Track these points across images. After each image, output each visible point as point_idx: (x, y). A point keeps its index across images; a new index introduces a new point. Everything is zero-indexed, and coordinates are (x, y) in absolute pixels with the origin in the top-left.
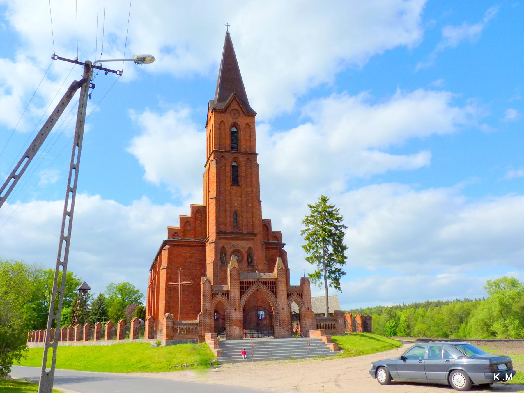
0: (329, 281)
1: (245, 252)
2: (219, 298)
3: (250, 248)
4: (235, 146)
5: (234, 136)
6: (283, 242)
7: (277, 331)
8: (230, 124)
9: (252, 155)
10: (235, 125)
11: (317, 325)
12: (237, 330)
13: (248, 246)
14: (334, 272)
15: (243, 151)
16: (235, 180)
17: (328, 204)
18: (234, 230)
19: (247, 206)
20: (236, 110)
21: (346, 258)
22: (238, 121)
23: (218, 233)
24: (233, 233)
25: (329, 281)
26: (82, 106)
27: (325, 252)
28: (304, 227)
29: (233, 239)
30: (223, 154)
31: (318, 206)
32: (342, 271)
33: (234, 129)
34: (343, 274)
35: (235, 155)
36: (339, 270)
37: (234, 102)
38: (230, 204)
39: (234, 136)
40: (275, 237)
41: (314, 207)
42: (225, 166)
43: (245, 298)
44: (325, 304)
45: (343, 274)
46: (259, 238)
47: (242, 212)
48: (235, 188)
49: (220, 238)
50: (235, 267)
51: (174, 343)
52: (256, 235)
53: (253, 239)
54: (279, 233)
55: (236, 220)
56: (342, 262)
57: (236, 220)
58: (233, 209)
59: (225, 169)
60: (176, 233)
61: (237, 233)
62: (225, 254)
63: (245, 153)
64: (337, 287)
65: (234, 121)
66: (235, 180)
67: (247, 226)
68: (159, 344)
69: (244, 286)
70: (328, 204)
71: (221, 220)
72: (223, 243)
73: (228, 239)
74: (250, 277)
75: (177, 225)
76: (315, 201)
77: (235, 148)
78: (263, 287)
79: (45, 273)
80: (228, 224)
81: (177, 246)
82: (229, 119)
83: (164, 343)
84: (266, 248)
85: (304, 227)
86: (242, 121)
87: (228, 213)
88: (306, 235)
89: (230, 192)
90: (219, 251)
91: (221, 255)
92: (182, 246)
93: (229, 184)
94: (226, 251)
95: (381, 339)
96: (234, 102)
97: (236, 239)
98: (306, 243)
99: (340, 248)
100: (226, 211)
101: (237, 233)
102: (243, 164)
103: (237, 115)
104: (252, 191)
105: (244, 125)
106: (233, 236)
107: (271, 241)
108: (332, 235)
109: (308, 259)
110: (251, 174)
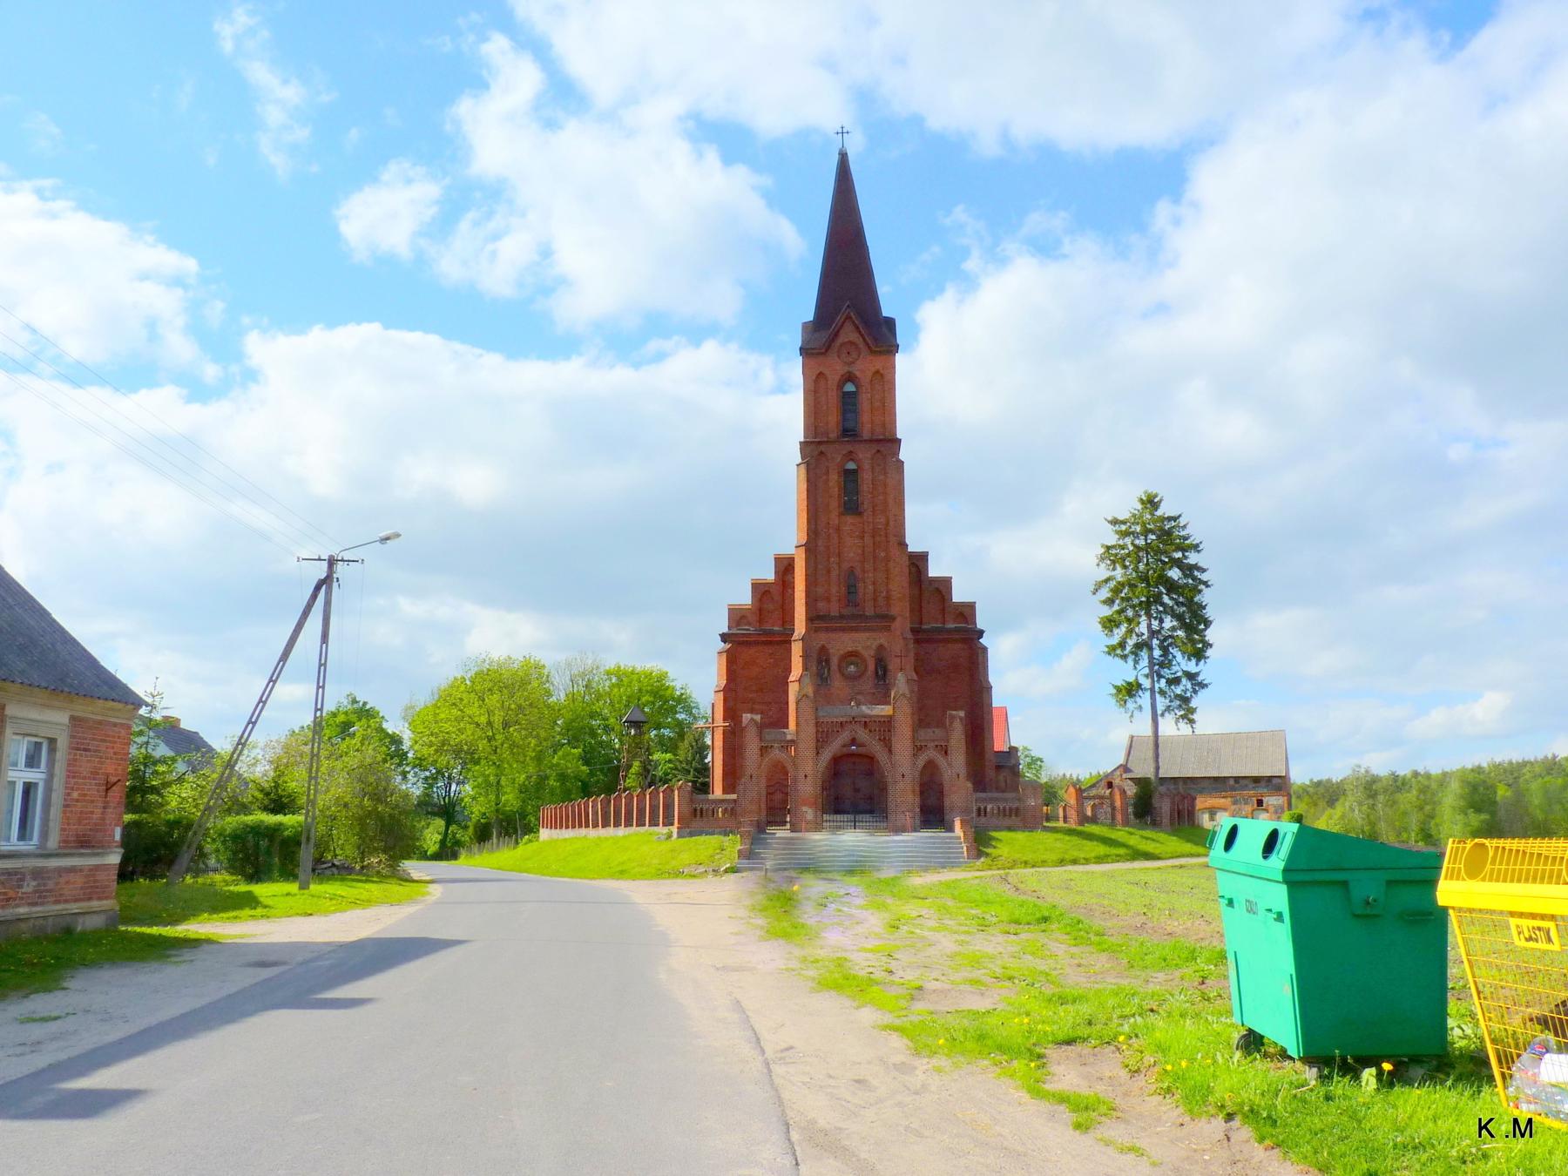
0: (1161, 703)
1: (869, 654)
2: (776, 754)
3: (881, 646)
4: (850, 425)
5: (848, 403)
6: (980, 625)
7: (892, 817)
8: (837, 378)
9: (888, 443)
10: (849, 378)
11: (979, 810)
12: (809, 813)
13: (875, 645)
14: (1175, 681)
15: (866, 435)
16: (852, 507)
17: (1159, 513)
18: (846, 612)
19: (875, 557)
20: (851, 343)
21: (1208, 645)
22: (856, 370)
23: (811, 619)
24: (842, 617)
25: (1161, 703)
26: (328, 603)
27: (1153, 634)
28: (1103, 572)
29: (843, 630)
30: (822, 448)
31: (1136, 519)
32: (1200, 679)
33: (850, 387)
34: (1203, 686)
35: (849, 447)
36: (1191, 676)
37: (848, 327)
38: (839, 555)
39: (848, 403)
40: (961, 614)
41: (1124, 522)
42: (827, 473)
43: (827, 755)
44: (1150, 754)
45: (1203, 686)
46: (902, 625)
47: (864, 571)
48: (850, 519)
49: (817, 630)
50: (806, 696)
51: (691, 835)
52: (893, 619)
53: (888, 629)
54: (971, 607)
55: (851, 589)
56: (1199, 655)
57: (851, 589)
58: (846, 566)
59: (827, 481)
60: (743, 617)
61: (854, 617)
62: (827, 661)
63: (871, 441)
64: (1188, 716)
65: (846, 369)
66: (852, 507)
67: (875, 600)
68: (669, 836)
69: (823, 736)
70: (1159, 513)
71: (820, 590)
72: (822, 639)
73: (835, 630)
74: (837, 713)
75: (745, 598)
76: (1127, 505)
77: (849, 433)
78: (863, 735)
79: (608, 673)
80: (834, 599)
81: (748, 644)
82: (835, 367)
83: (675, 835)
84: (917, 641)
85: (1103, 572)
86: (865, 367)
87: (834, 573)
88: (1105, 593)
89: (838, 529)
90: (815, 656)
91: (819, 662)
92: (757, 643)
93: (834, 515)
94: (828, 655)
95: (1149, 847)
96: (848, 327)
97: (853, 629)
98: (1107, 611)
99: (1194, 621)
100: (829, 571)
101: (854, 617)
102: (866, 465)
103: (854, 355)
104: (887, 524)
105: (869, 374)
106: (843, 624)
107: (951, 626)
108: (1172, 587)
109: (1111, 650)
110: (885, 485)
